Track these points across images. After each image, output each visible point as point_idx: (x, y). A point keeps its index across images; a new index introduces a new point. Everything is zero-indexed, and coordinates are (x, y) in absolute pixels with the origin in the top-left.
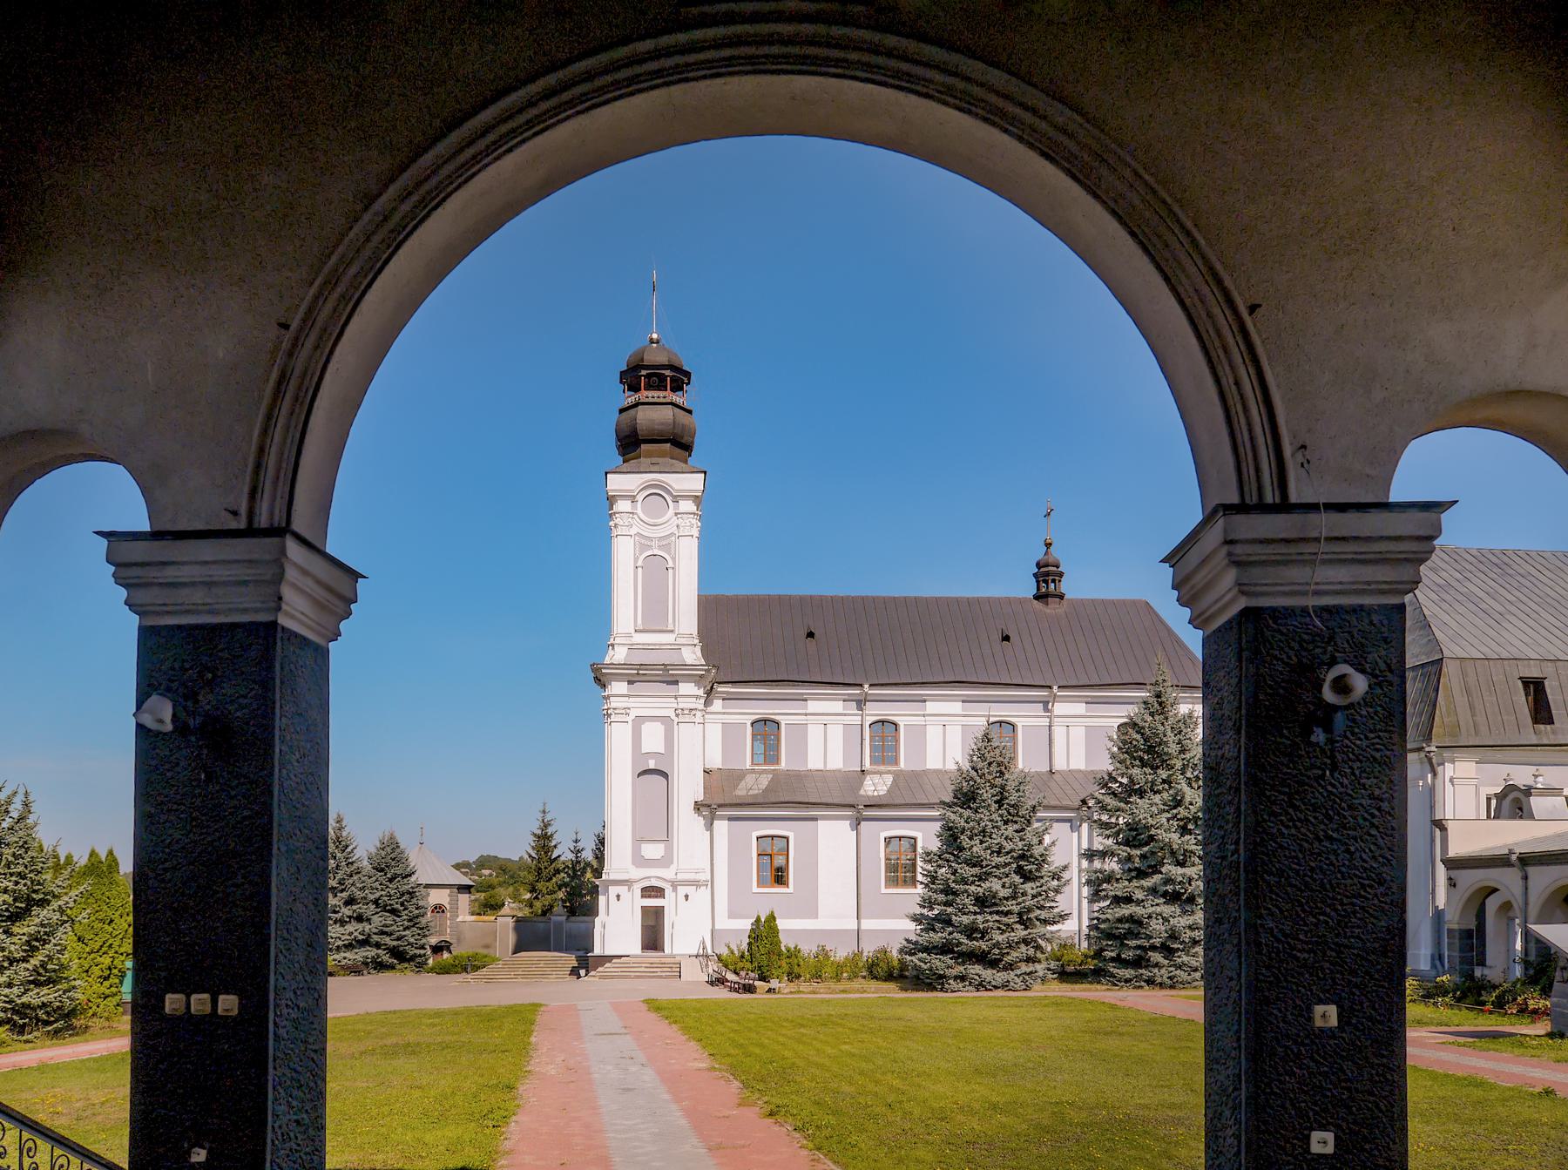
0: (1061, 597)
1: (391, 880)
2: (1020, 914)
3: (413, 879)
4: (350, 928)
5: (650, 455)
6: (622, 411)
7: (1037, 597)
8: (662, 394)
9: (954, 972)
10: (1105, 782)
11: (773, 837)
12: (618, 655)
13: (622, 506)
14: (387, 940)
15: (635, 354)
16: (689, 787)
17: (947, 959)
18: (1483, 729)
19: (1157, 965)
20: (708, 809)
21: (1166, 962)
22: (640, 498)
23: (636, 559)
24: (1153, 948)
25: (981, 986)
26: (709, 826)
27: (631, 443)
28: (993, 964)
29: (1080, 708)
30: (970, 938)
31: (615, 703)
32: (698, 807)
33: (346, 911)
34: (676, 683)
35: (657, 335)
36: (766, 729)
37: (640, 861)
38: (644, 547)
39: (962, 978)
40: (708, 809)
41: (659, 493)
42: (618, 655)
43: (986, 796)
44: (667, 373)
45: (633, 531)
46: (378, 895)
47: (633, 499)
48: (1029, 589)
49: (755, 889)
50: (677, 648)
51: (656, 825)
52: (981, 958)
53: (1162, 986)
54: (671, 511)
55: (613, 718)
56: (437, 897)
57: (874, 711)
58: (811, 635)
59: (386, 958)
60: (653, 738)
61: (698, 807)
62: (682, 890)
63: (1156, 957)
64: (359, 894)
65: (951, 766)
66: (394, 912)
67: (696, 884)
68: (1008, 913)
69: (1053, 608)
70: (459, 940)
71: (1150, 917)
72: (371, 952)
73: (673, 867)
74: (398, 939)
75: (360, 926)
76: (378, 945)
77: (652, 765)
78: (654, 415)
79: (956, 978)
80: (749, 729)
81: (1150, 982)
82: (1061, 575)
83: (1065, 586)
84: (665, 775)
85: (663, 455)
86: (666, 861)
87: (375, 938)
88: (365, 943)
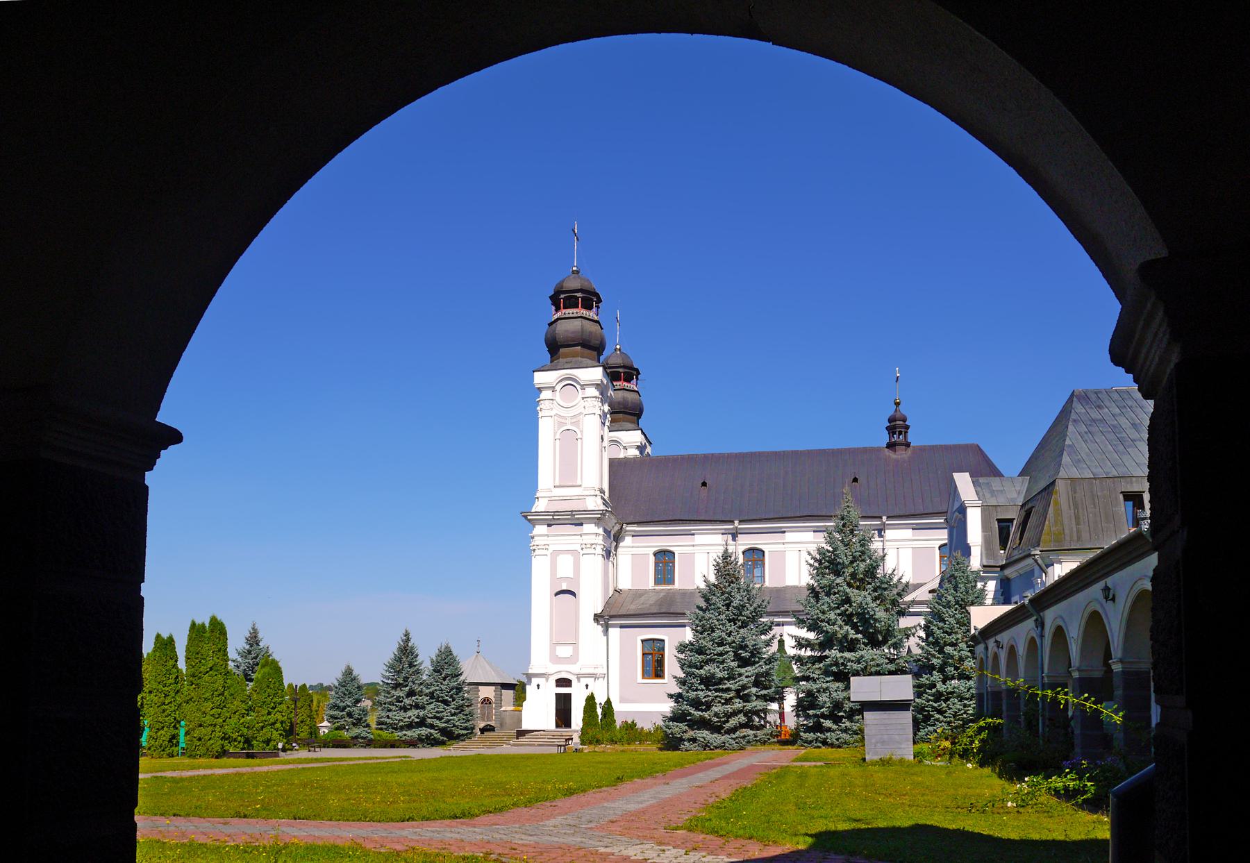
0: (908, 445)
1: (444, 679)
2: (738, 691)
3: (462, 678)
4: (410, 713)
5: (566, 356)
6: (550, 325)
7: (891, 446)
8: (575, 310)
9: (686, 736)
10: (812, 589)
11: (654, 640)
12: (540, 506)
13: (545, 395)
14: (436, 722)
15: (557, 281)
16: (592, 600)
17: (683, 726)
18: (1085, 535)
19: (829, 730)
20: (604, 619)
21: (835, 727)
22: (558, 388)
23: (555, 433)
24: (823, 716)
25: (706, 746)
26: (606, 632)
27: (557, 349)
28: (717, 729)
29: (907, 533)
30: (697, 709)
31: (537, 541)
32: (597, 618)
33: (407, 701)
34: (581, 524)
35: (575, 266)
36: (664, 559)
37: (556, 659)
38: (561, 424)
39: (694, 740)
40: (604, 619)
41: (571, 382)
42: (540, 506)
43: (733, 603)
44: (579, 295)
45: (552, 413)
46: (433, 688)
47: (553, 389)
48: (885, 438)
49: (640, 679)
50: (582, 498)
51: (566, 636)
52: (703, 724)
53: (832, 746)
54: (580, 396)
55: (537, 552)
56: (486, 692)
57: (745, 542)
58: (704, 484)
59: (437, 735)
60: (565, 567)
61: (597, 618)
62: (584, 681)
63: (828, 723)
64: (416, 688)
65: (803, 583)
66: (446, 703)
67: (595, 677)
68: (728, 690)
69: (901, 454)
70: (502, 725)
71: (819, 691)
72: (424, 731)
73: (579, 664)
74: (448, 722)
75: (416, 712)
76: (432, 726)
77: (564, 588)
78: (573, 322)
79: (689, 740)
80: (652, 558)
81: (825, 743)
82: (907, 427)
83: (912, 437)
84: (573, 593)
85: (575, 355)
86: (573, 659)
87: (429, 721)
88: (422, 723)
